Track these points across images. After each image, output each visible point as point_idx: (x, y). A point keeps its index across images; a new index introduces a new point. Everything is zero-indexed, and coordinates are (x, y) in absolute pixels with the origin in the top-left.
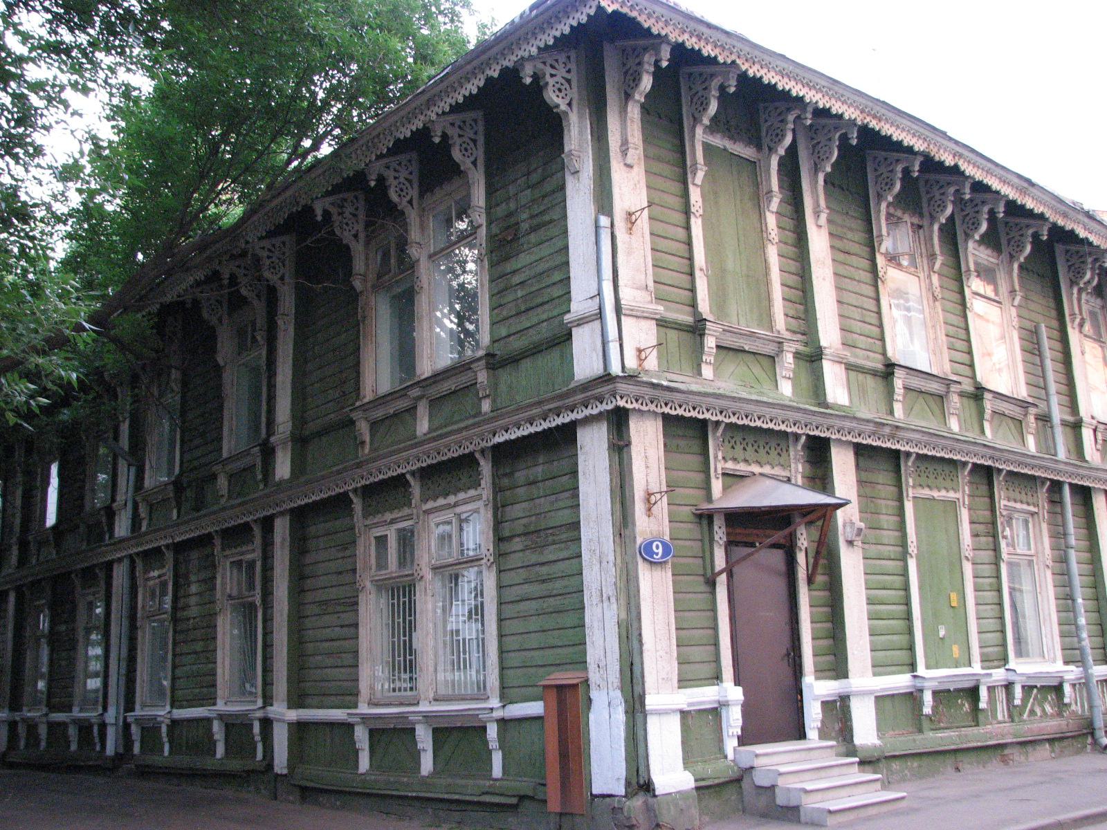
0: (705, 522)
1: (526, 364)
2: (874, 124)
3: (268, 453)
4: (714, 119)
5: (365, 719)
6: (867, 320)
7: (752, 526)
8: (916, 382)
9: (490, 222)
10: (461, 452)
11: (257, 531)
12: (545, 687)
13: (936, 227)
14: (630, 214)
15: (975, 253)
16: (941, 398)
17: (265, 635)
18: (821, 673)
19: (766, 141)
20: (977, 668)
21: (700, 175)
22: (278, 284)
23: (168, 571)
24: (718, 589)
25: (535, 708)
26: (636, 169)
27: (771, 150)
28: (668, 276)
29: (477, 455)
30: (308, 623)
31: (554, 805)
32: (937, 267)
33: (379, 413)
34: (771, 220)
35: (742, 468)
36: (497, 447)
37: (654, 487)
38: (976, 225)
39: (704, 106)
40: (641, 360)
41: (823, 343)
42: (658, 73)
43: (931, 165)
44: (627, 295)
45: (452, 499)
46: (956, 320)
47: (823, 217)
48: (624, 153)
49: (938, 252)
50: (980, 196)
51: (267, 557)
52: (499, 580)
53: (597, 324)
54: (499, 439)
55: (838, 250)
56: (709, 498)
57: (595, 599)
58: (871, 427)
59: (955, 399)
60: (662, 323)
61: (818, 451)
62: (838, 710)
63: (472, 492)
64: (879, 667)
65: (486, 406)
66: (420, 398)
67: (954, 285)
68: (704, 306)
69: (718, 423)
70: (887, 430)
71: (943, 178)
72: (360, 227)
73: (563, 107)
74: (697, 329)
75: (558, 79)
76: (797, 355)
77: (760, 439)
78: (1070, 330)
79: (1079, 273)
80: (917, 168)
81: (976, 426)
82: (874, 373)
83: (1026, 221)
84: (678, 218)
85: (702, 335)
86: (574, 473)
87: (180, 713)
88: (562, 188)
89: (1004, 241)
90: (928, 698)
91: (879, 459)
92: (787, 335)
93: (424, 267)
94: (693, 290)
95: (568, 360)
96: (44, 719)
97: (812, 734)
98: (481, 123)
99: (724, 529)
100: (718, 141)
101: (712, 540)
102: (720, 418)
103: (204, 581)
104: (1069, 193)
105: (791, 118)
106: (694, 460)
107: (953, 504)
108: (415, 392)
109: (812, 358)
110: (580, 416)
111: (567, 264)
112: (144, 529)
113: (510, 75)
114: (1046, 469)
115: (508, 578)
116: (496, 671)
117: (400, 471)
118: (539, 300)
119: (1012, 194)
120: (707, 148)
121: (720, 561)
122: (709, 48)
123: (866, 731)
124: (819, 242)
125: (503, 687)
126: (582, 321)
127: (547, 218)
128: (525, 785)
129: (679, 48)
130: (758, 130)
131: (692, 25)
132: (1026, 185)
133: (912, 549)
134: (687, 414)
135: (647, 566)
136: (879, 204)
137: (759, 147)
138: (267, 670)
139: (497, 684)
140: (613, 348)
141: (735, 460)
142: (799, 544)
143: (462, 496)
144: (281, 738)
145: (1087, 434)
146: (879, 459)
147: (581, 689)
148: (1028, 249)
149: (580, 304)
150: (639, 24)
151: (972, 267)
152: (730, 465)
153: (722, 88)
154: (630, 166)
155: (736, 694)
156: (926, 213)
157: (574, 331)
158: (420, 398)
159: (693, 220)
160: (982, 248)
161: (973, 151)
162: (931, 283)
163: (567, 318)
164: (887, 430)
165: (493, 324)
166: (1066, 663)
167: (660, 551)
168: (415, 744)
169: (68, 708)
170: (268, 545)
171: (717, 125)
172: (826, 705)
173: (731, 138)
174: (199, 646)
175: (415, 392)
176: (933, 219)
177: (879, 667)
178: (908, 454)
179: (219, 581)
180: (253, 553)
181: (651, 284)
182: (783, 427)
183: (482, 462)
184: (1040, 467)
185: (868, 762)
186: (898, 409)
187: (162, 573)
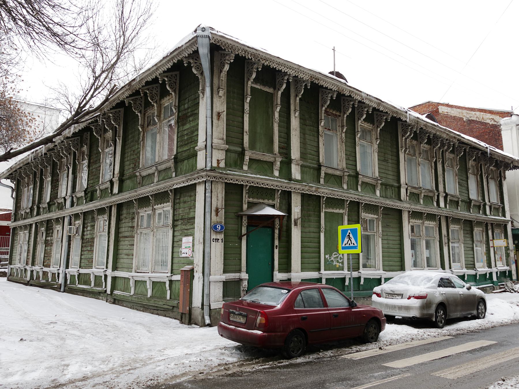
0: (240, 218)
8: (330, 171)
13: (345, 116)
18: (280, 271)
19: (277, 87)
24: (243, 241)
26: (223, 97)
27: (279, 90)
32: (344, 130)
34: (277, 115)
35: (255, 200)
37: (220, 206)
39: (251, 75)
41: (293, 158)
43: (340, 95)
44: (215, 141)
45: (162, 205)
47: (297, 114)
54: (174, 187)
56: (242, 210)
57: (197, 243)
61: (287, 195)
69: (247, 185)
74: (242, 154)
76: (281, 162)
77: (265, 193)
78: (400, 153)
80: (335, 96)
82: (314, 168)
85: (244, 155)
94: (243, 139)
96: (41, 270)
97: (274, 203)
98: (178, 76)
99: (246, 221)
101: (241, 225)
107: (342, 215)
109: (287, 163)
110: (197, 182)
121: (244, 231)
124: (295, 123)
132: (380, 102)
135: (215, 233)
136: (322, 108)
137: (275, 88)
138: (108, 258)
140: (209, 155)
142: (276, 227)
143: (165, 204)
145: (403, 191)
148: (383, 124)
151: (359, 130)
152: (251, 200)
155: (244, 276)
156: (342, 110)
157: (198, 152)
159: (245, 115)
162: (342, 136)
163: (196, 148)
167: (220, 228)
173: (263, 85)
174: (89, 248)
176: (344, 113)
179: (96, 226)
181: (225, 138)
187: (79, 222)
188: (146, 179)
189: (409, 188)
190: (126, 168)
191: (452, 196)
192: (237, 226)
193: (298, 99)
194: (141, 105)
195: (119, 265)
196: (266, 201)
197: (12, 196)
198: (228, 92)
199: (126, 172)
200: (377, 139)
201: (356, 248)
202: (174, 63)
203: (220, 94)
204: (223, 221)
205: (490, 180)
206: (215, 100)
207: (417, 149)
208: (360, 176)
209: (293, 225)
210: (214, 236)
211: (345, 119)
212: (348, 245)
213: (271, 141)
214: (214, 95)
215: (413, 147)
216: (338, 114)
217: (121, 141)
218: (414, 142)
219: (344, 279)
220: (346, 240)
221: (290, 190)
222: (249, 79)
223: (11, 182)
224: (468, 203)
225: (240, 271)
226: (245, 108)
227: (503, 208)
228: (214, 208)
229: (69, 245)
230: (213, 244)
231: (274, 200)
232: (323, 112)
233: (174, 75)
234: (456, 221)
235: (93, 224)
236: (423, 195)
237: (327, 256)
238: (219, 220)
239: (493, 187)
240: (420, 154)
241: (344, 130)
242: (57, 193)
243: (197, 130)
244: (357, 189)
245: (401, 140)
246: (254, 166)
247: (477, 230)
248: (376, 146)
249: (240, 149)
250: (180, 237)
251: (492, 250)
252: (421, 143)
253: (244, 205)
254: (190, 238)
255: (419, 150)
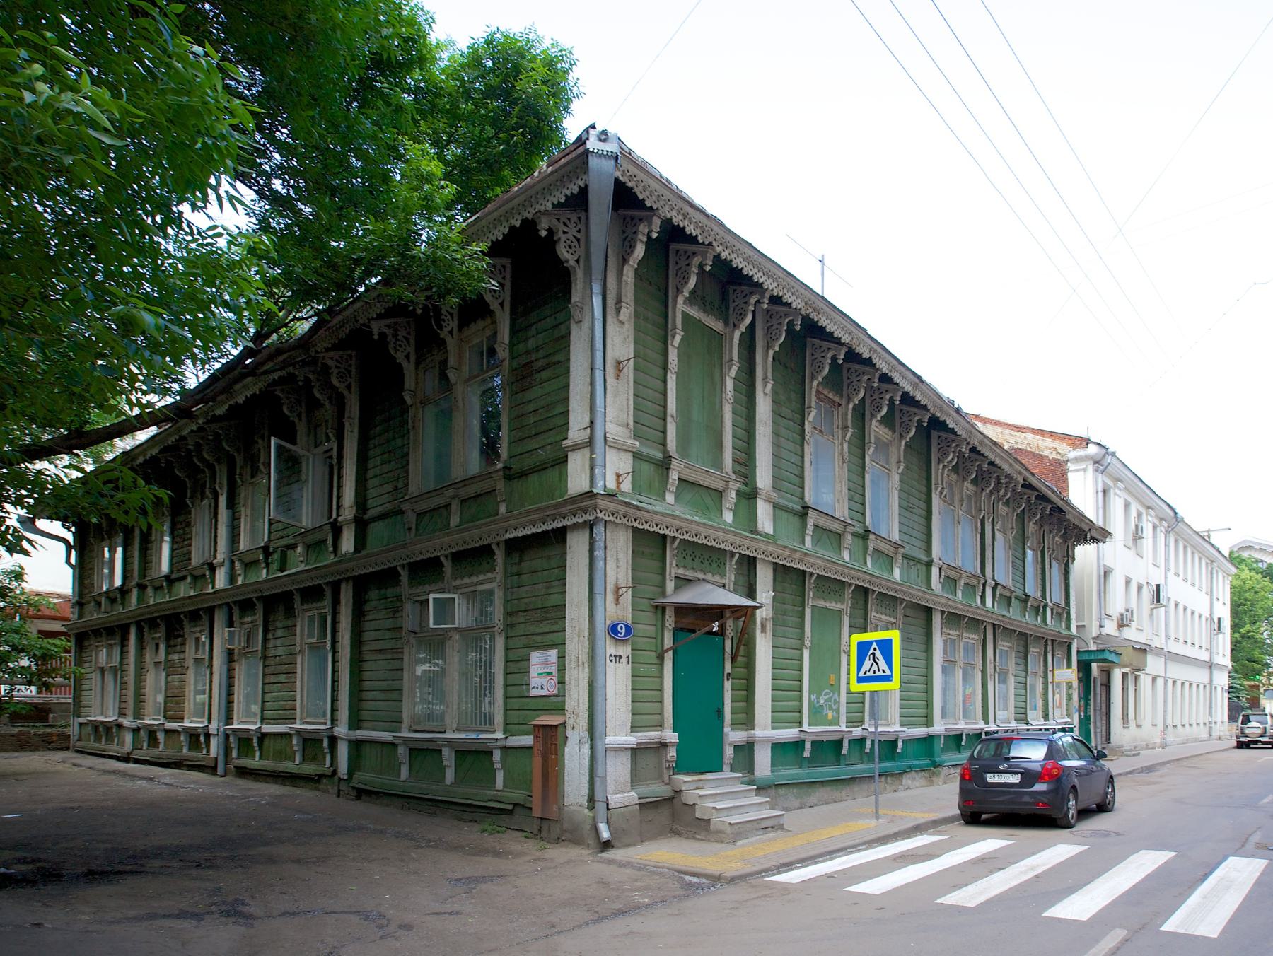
0: (659, 612)
1: (534, 478)
2: (814, 316)
3: (337, 530)
4: (693, 292)
5: (405, 740)
6: (791, 475)
7: (696, 619)
8: (823, 522)
9: (513, 358)
10: (481, 543)
11: (328, 593)
12: (535, 726)
13: (851, 406)
14: (619, 363)
15: (876, 429)
16: (839, 536)
17: (334, 672)
18: (735, 725)
19: (732, 319)
20: (843, 728)
21: (678, 339)
22: (346, 393)
23: (259, 617)
25: (528, 740)
26: (627, 325)
28: (645, 419)
29: (494, 547)
30: (366, 666)
31: (537, 812)
32: (848, 437)
33: (423, 506)
34: (730, 384)
35: (690, 574)
36: (508, 541)
37: (622, 582)
38: (879, 409)
40: (619, 483)
41: (759, 485)
42: (650, 243)
46: (856, 479)
47: (769, 386)
48: (618, 311)
49: (735, 357)
50: (886, 386)
51: (335, 613)
52: (506, 644)
53: (587, 451)
54: (510, 535)
55: (777, 414)
56: (664, 594)
58: (786, 552)
59: (850, 537)
60: (637, 456)
61: (749, 564)
62: (746, 750)
63: (489, 575)
64: (776, 723)
65: (503, 509)
66: (453, 497)
67: (858, 451)
68: (672, 445)
70: (798, 556)
71: (861, 368)
72: (411, 350)
73: (572, 263)
74: (664, 464)
75: (569, 236)
76: (738, 493)
77: (706, 556)
79: (945, 455)
81: (861, 558)
82: (794, 513)
83: (916, 410)
84: (658, 371)
85: (668, 469)
86: (563, 567)
87: (267, 728)
88: (567, 335)
89: (898, 422)
90: (808, 746)
91: (791, 578)
92: (733, 476)
93: (459, 390)
94: (664, 432)
95: (563, 477)
98: (508, 270)
100: (694, 312)
101: (663, 626)
102: (676, 534)
103: (287, 628)
104: (946, 391)
105: (753, 301)
106: (655, 564)
107: (839, 613)
108: (450, 492)
109: (749, 495)
111: (567, 399)
112: (240, 582)
113: (529, 226)
114: (905, 593)
115: (512, 643)
116: (502, 712)
117: (436, 554)
118: (545, 427)
119: (908, 388)
120: (686, 316)
121: (668, 642)
122: (692, 227)
123: (763, 762)
124: (764, 407)
125: (506, 724)
126: (576, 447)
127: (556, 359)
128: (518, 796)
129: (667, 223)
130: (727, 308)
131: (681, 204)
133: (808, 643)
134: (651, 529)
137: (726, 323)
138: (334, 700)
139: (502, 721)
141: (684, 567)
143: (482, 577)
144: (343, 751)
145: (935, 571)
146: (791, 578)
147: (560, 729)
148: (913, 431)
149: (576, 432)
150: (635, 194)
152: (681, 571)
153: (701, 266)
154: (622, 323)
155: (671, 737)
157: (571, 456)
158: (453, 497)
159: (669, 375)
160: (882, 427)
161: (884, 348)
164: (798, 556)
165: (510, 443)
166: (901, 725)
168: (442, 761)
169: (181, 719)
170: (336, 602)
171: (694, 298)
172: (737, 748)
173: (705, 311)
175: (450, 492)
176: (849, 399)
177: (776, 723)
178: (812, 574)
179: (298, 628)
180: (326, 606)
181: (631, 423)
182: (722, 546)
183: (497, 552)
184: (901, 591)
185: (762, 789)
186: (808, 540)
188: (426, 519)
189: (945, 567)
190: (372, 493)
191: (1004, 587)
192: (653, 628)
193: (771, 353)
194: (408, 340)
195: (365, 715)
196: (709, 577)
197: (68, 561)
198: (637, 315)
199: (370, 503)
200: (899, 462)
201: (888, 678)
202: (512, 228)
203: (621, 318)
204: (630, 616)
205: (1054, 562)
206: (609, 329)
207: (956, 490)
208: (872, 537)
209: (758, 632)
210: (612, 649)
211: (850, 412)
212: (871, 674)
213: (719, 445)
214: (609, 319)
215: (950, 486)
216: (837, 399)
217: (356, 430)
218: (954, 477)
219: (839, 743)
220: (867, 663)
221: (755, 555)
222: (679, 291)
223: (63, 526)
224: (1025, 599)
225: (661, 726)
226: (670, 360)
227: (1068, 614)
228: (610, 587)
229: (230, 670)
230: (611, 666)
231: (723, 575)
232: (814, 390)
233: (498, 267)
234: (1009, 632)
235: (289, 623)
236: (963, 581)
237: (813, 697)
238: (620, 613)
239: (1055, 572)
240: (961, 501)
241: (848, 437)
242: (190, 553)
243: (566, 400)
244: (803, 543)
245: (937, 471)
246: (688, 496)
247: (1034, 651)
248: (897, 477)
249: (660, 455)
250: (522, 652)
251: (1050, 686)
252: (964, 479)
253: (668, 581)
254: (553, 654)
255: (961, 493)
